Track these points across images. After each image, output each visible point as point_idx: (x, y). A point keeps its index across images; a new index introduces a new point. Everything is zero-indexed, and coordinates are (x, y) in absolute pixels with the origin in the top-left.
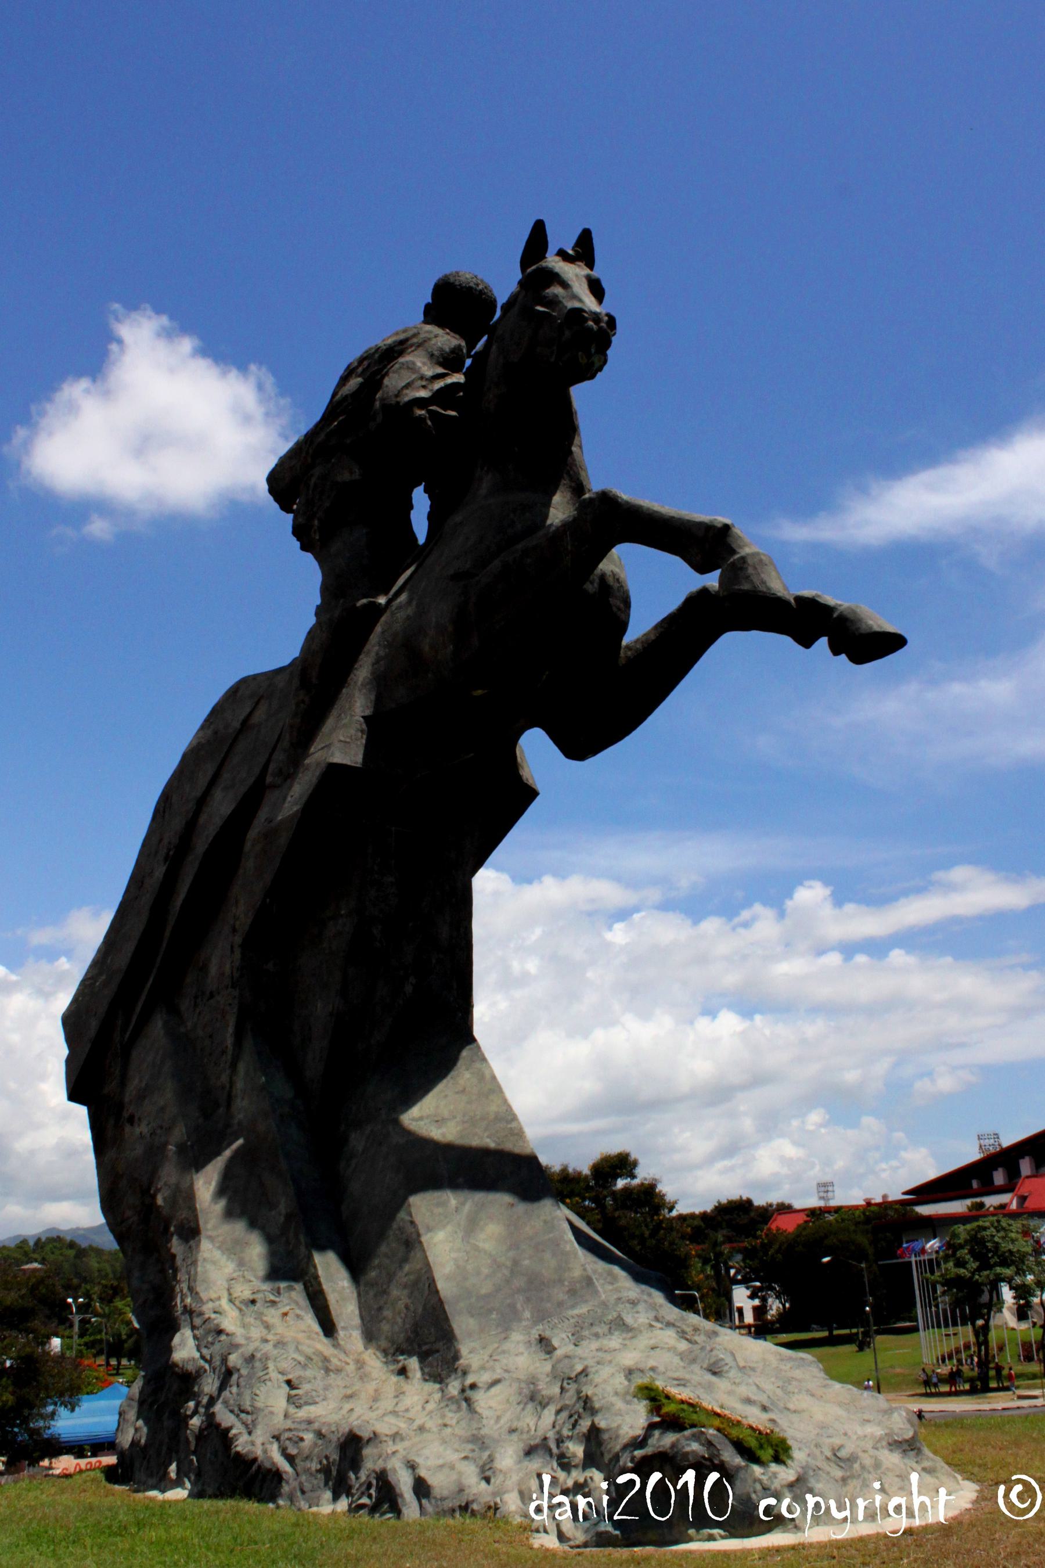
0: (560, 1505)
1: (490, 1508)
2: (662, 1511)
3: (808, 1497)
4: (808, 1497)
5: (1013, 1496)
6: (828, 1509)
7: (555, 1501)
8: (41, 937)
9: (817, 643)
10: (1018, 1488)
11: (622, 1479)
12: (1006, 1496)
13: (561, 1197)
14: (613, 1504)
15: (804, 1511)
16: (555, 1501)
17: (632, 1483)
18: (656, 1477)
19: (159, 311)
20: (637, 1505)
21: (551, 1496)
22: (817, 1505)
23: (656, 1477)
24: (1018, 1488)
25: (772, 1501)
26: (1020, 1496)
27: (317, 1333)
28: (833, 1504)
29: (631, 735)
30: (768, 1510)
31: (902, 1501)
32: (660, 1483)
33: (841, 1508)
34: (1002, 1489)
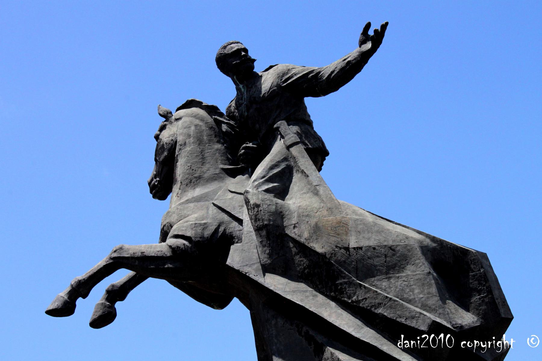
0: (407, 343)
1: (332, 254)
2: (434, 344)
3: (475, 341)
4: (475, 341)
5: (532, 341)
6: (480, 344)
7: (405, 342)
8: (180, 242)
9: (309, 111)
10: (533, 339)
11: (423, 336)
12: (530, 341)
13: (283, 162)
14: (421, 344)
15: (474, 345)
16: (405, 342)
17: (426, 337)
18: (433, 336)
19: (270, 255)
20: (428, 343)
21: (404, 341)
22: (477, 344)
23: (433, 336)
24: (533, 339)
25: (465, 342)
26: (534, 341)
27: (382, 345)
28: (481, 343)
29: (223, 74)
30: (464, 345)
31: (501, 342)
32: (434, 337)
33: (484, 344)
34: (528, 339)
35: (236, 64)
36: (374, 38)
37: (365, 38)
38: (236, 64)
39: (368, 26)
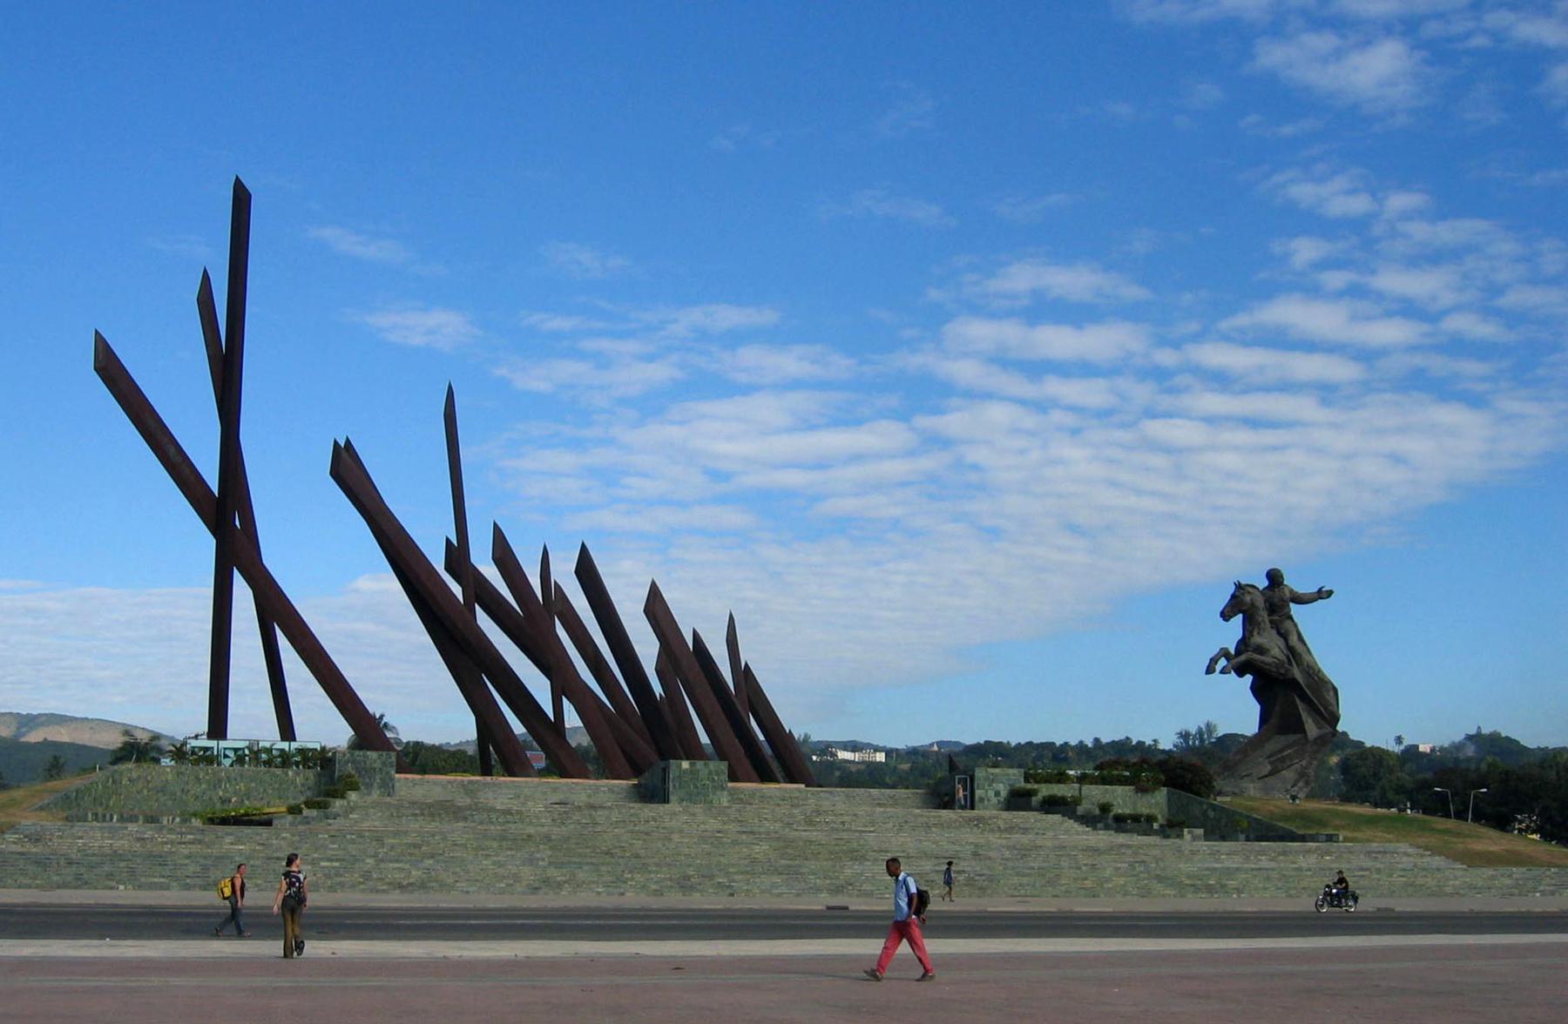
38: (1274, 578)
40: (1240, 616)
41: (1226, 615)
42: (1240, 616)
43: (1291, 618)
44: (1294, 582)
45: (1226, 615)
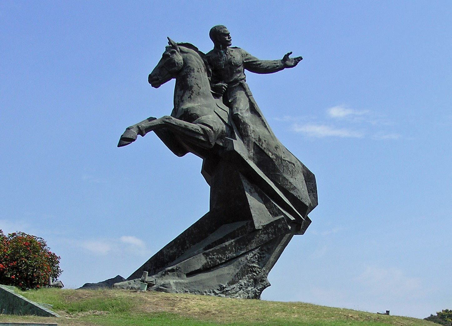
35: (219, 36)
36: (286, 63)
37: (286, 57)
39: (291, 53)
40: (173, 81)
41: (156, 80)
42: (173, 81)
43: (242, 87)
44: (243, 44)
45: (156, 80)
